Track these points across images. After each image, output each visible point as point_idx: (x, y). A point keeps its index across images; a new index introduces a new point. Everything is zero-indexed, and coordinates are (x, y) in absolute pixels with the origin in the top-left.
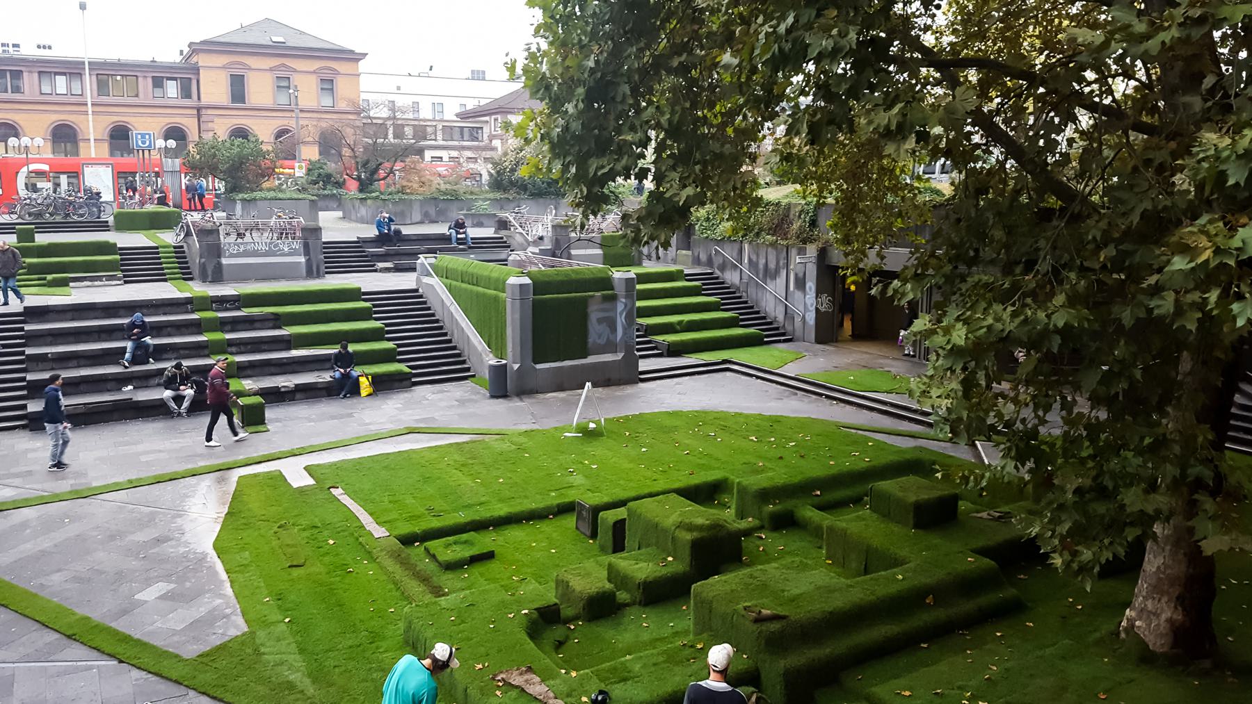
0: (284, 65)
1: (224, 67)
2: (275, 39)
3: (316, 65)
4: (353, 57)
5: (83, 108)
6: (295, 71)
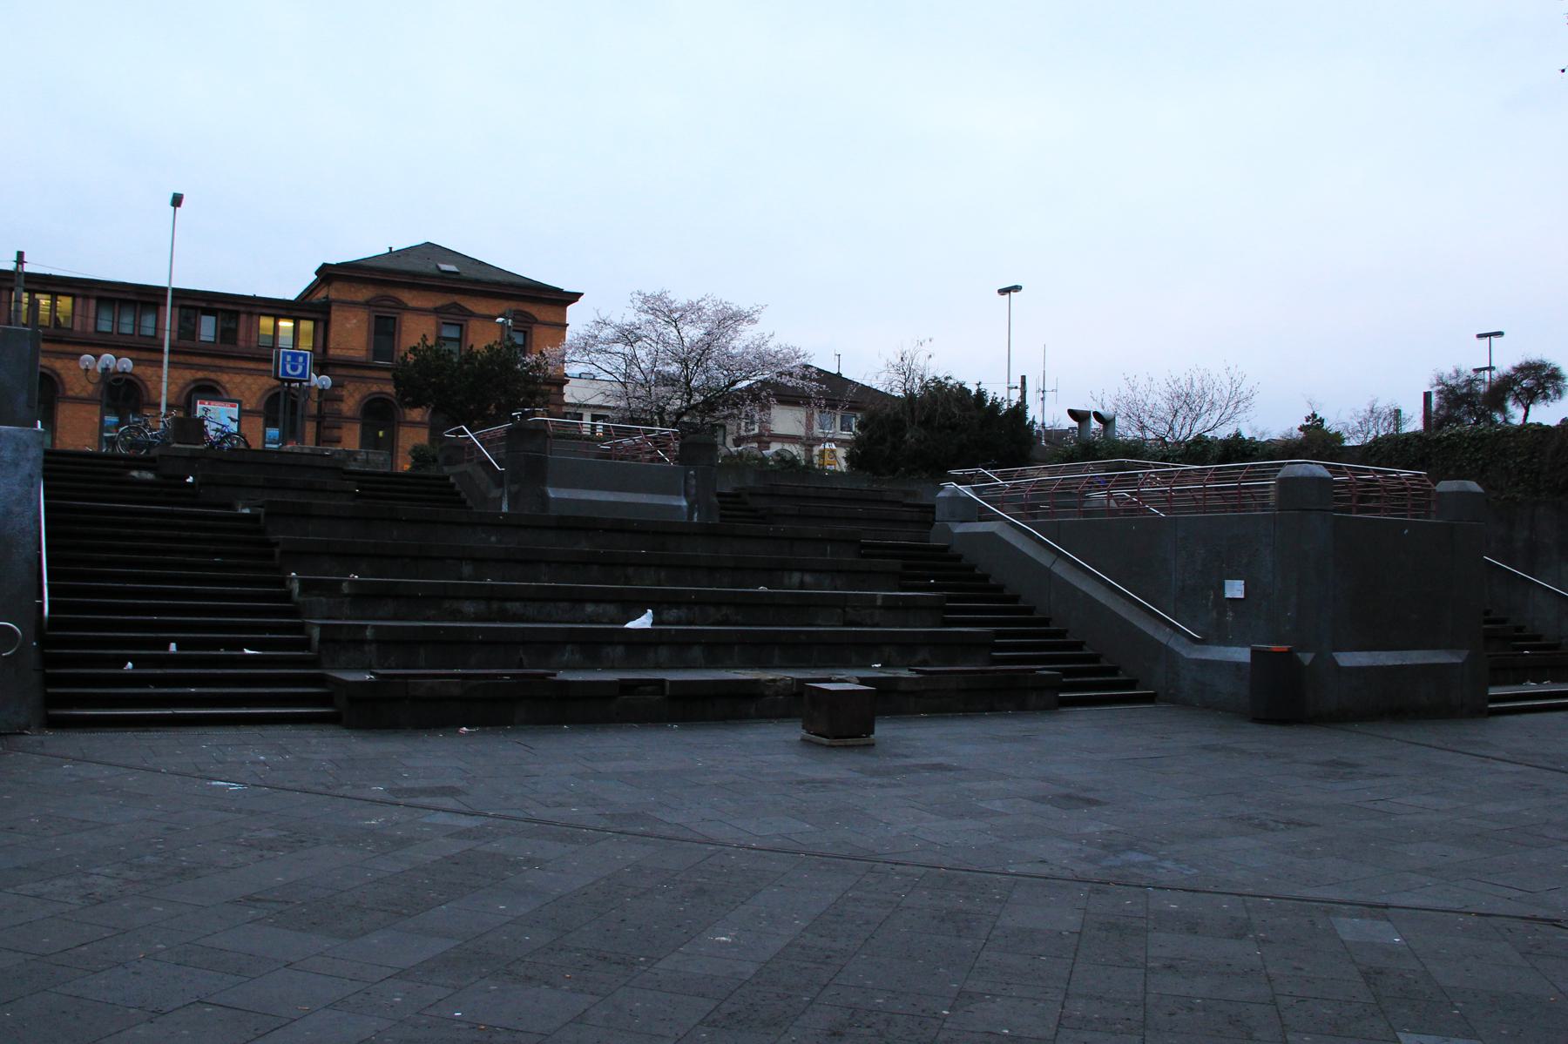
0: (455, 305)
1: (367, 304)
2: (444, 267)
3: (439, 300)
4: (564, 299)
5: (154, 356)
6: (472, 315)
